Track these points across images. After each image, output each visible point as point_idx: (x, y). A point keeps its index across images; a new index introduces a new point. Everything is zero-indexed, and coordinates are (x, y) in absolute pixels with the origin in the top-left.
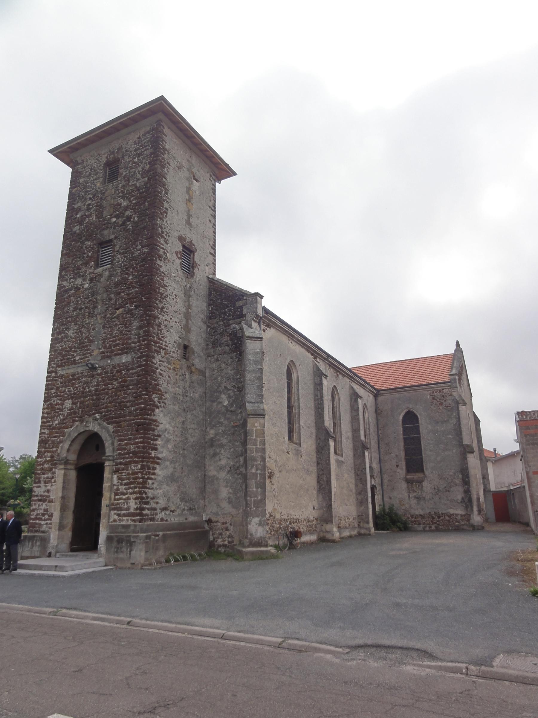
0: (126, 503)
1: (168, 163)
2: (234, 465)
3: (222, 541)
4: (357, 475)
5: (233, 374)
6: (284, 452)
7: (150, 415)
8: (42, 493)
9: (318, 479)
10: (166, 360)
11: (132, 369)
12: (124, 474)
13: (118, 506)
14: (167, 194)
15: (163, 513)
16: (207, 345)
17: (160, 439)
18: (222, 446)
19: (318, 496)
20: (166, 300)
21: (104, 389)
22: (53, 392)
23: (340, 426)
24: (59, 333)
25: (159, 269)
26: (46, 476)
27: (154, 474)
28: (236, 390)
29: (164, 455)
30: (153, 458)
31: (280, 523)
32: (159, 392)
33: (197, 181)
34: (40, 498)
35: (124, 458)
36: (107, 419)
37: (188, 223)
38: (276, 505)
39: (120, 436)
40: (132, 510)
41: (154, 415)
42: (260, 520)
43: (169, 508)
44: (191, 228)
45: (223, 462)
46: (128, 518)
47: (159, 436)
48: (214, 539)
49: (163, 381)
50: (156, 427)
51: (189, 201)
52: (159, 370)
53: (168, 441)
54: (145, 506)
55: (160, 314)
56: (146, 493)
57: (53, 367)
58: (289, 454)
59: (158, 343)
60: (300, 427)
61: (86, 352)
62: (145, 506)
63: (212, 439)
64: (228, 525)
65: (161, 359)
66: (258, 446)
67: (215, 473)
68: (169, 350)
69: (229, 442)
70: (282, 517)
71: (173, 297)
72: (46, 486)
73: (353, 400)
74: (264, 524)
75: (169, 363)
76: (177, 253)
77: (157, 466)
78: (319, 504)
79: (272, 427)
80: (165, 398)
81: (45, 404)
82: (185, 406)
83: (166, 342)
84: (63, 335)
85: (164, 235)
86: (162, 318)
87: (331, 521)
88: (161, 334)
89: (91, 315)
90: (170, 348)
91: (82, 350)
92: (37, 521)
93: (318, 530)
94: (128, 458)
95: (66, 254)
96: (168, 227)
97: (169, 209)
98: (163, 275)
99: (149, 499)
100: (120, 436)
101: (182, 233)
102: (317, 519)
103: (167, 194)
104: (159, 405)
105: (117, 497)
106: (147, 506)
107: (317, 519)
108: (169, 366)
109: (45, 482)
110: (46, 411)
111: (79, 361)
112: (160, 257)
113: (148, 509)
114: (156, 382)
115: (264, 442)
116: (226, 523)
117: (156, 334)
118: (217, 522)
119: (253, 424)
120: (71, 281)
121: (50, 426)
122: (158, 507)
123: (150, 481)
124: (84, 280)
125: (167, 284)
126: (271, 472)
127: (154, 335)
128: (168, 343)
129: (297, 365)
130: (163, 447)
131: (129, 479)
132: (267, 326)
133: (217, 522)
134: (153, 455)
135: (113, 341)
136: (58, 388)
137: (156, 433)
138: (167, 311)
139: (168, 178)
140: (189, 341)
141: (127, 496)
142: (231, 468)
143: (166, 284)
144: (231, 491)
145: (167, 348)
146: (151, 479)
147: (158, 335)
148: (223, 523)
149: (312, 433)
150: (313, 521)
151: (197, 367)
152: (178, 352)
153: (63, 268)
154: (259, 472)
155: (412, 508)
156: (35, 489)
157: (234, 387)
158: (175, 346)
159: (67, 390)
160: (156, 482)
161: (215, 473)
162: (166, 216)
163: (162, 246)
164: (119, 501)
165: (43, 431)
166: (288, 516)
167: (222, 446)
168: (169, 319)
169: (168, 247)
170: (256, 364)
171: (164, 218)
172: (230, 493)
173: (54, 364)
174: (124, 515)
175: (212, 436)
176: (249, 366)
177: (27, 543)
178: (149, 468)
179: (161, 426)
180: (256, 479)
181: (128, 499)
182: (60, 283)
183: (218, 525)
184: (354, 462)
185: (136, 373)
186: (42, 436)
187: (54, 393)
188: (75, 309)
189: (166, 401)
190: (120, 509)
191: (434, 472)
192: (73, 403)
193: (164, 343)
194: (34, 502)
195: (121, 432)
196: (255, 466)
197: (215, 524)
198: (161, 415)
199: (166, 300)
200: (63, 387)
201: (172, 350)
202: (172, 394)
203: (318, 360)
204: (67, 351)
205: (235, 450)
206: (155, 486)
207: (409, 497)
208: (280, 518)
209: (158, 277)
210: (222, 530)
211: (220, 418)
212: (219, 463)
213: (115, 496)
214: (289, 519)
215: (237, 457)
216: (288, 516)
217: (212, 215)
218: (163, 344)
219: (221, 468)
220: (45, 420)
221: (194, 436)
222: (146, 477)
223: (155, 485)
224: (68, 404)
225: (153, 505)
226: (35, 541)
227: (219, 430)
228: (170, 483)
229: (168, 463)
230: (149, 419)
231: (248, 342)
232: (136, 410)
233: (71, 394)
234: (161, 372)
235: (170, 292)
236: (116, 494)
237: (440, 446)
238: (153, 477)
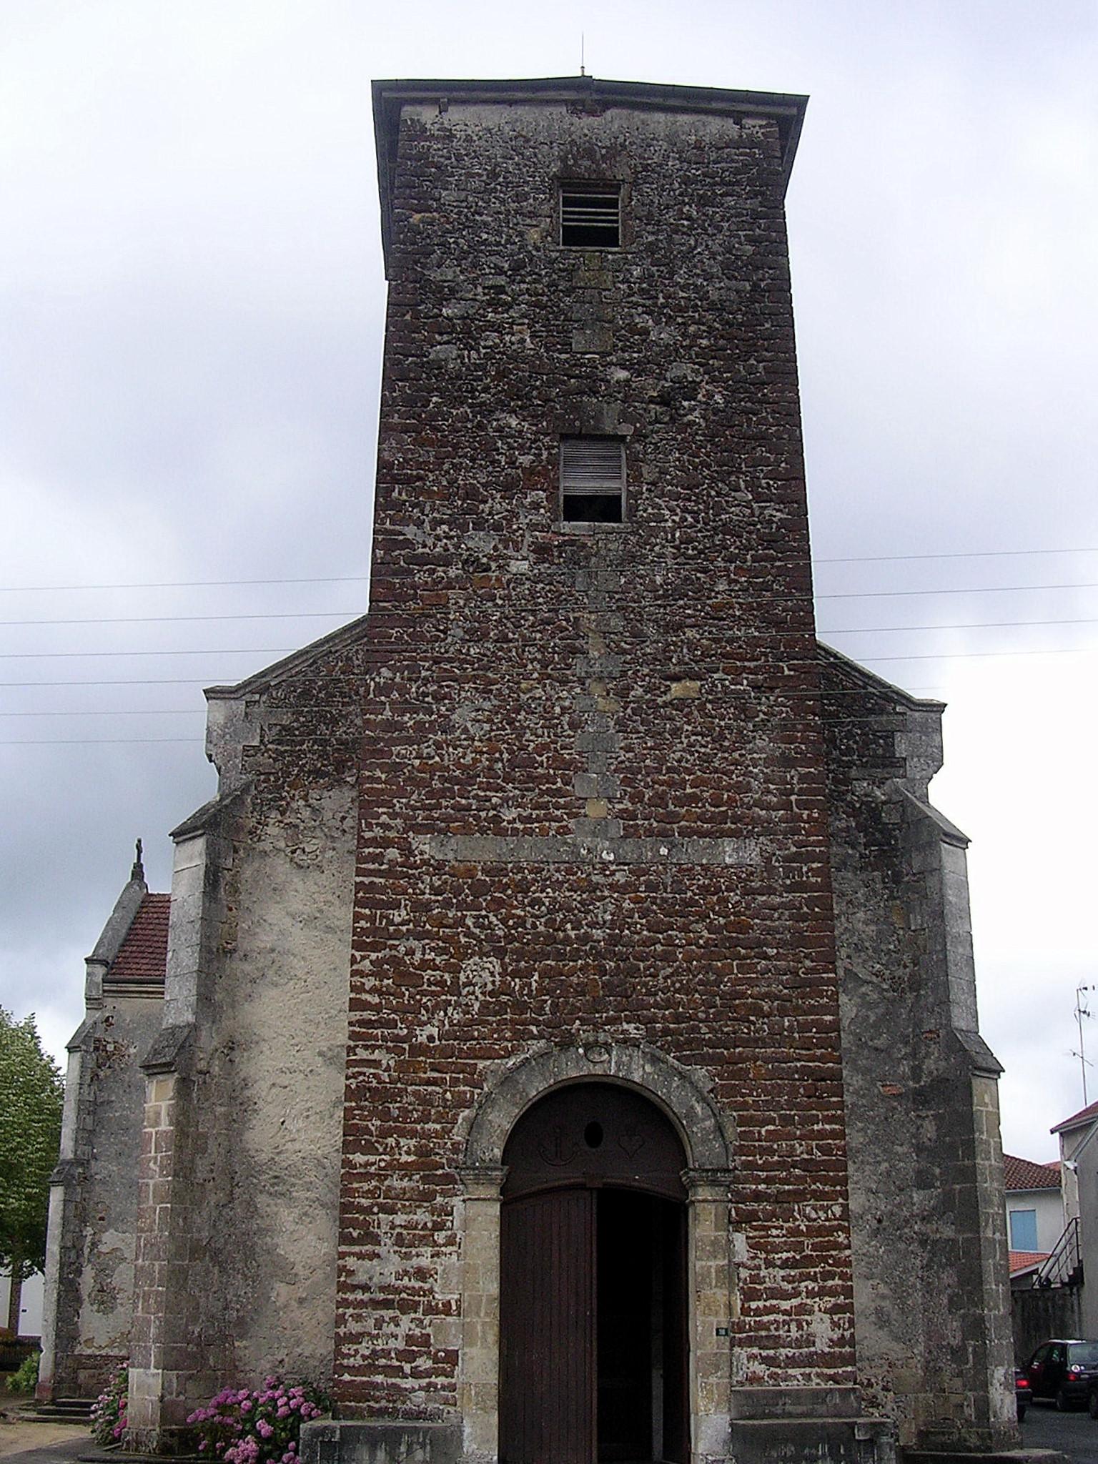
13: (763, 1333)
35: (767, 1181)
40: (821, 1346)
46: (808, 1370)
64: (877, 1389)
94: (785, 1181)
105: (753, 1305)
109: (400, 1241)
174: (792, 1362)
181: (802, 1309)
226: (403, 1448)
231: (948, 852)
236: (750, 1295)
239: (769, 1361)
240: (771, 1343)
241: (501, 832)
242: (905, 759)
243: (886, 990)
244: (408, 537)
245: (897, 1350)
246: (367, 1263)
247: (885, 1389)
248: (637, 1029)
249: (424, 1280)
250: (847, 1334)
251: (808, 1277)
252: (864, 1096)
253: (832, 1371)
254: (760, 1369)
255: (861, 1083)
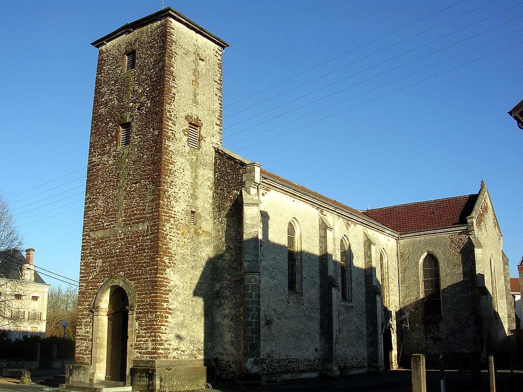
0: (145, 344)
1: (175, 53)
2: (235, 314)
3: (226, 376)
4: (368, 318)
5: (234, 235)
6: (283, 301)
7: (162, 274)
8: (83, 334)
9: (321, 324)
10: (175, 227)
11: (146, 236)
12: (143, 321)
13: (140, 346)
14: (174, 81)
15: (175, 352)
16: (214, 208)
17: (170, 294)
18: (226, 298)
19: (320, 339)
20: (174, 174)
21: (126, 251)
22: (87, 253)
23: (351, 273)
24: (91, 202)
25: (168, 149)
26: (85, 320)
27: (166, 322)
28: (237, 249)
29: (174, 306)
30: (166, 309)
31: (278, 362)
32: (169, 255)
33: (203, 60)
34: (82, 338)
35: (142, 309)
36: (129, 276)
37: (195, 102)
38: (274, 347)
39: (139, 291)
40: (150, 350)
41: (166, 274)
42: (255, 359)
43: (180, 349)
44: (197, 106)
45: (227, 311)
46: (147, 355)
47: (170, 291)
48: (220, 374)
49: (173, 245)
50: (167, 284)
51: (195, 82)
52: (169, 236)
53: (178, 294)
54: (159, 347)
55: (169, 187)
56: (160, 337)
57: (86, 231)
58: (289, 303)
59: (169, 213)
60: (302, 278)
61: (111, 219)
62: (159, 347)
63: (217, 292)
64: (231, 363)
65: (170, 227)
66: (254, 299)
67: (221, 320)
68: (178, 218)
69: (231, 294)
70: (281, 357)
71: (180, 171)
72: (86, 329)
73: (366, 247)
74: (258, 363)
75: (177, 229)
76: (184, 131)
77: (169, 316)
78: (321, 346)
79: (271, 280)
80: (174, 259)
81: (82, 262)
82: (192, 264)
83: (175, 211)
84: (94, 204)
85: (172, 118)
86: (171, 191)
87: (332, 361)
88: (170, 205)
89: (114, 188)
90: (179, 216)
91: (109, 218)
92: (81, 355)
93: (320, 369)
94: (145, 309)
95: (95, 133)
96: (176, 110)
97: (177, 94)
98: (171, 153)
99: (163, 342)
100: (139, 291)
101: (189, 112)
102: (319, 360)
103: (174, 81)
104: (169, 265)
105: (138, 339)
106: (162, 347)
107: (319, 360)
108: (178, 232)
109: (85, 326)
110: (83, 268)
111: (107, 227)
112: (169, 138)
113: (162, 349)
114: (166, 246)
115: (259, 296)
116: (230, 362)
117: (166, 206)
118: (223, 360)
119: (251, 279)
120: (98, 158)
121: (86, 280)
122: (171, 347)
123: (163, 328)
124: (109, 157)
125: (175, 161)
126: (269, 320)
127: (164, 207)
128: (176, 212)
129: (300, 220)
130: (173, 300)
131: (146, 325)
132: (267, 190)
133: (223, 360)
134: (165, 306)
135: (132, 211)
136: (91, 249)
137: (167, 288)
138: (175, 184)
139: (175, 66)
140: (196, 207)
141: (146, 339)
142: (233, 317)
143: (174, 161)
144: (233, 335)
145: (176, 216)
146: (165, 325)
147: (167, 206)
148: (227, 362)
149: (315, 283)
150: (315, 361)
151: (204, 229)
152: (186, 219)
153: (92, 145)
154: (254, 320)
155: (428, 348)
156: (78, 330)
157: (235, 246)
158: (184, 214)
159: (98, 251)
160: (168, 328)
161: (221, 320)
162: (174, 101)
163: (170, 128)
164: (140, 343)
165: (81, 284)
166: (287, 357)
167: (226, 298)
168: (178, 191)
169: (175, 128)
170: (253, 227)
171: (172, 102)
172: (232, 337)
173: (87, 229)
174: (144, 353)
175: (218, 289)
176: (247, 229)
177: (75, 372)
178: (162, 317)
179: (172, 283)
180: (252, 326)
181: (147, 341)
182: (90, 159)
183: (223, 363)
184: (367, 306)
185: (149, 239)
186: (81, 288)
187: (88, 253)
188: (103, 182)
189: (175, 262)
190: (141, 348)
191: (450, 314)
192: (103, 263)
193: (173, 213)
194: (78, 341)
195: (139, 288)
196: (251, 316)
197: (220, 362)
198: (172, 273)
199: (174, 174)
200: (95, 248)
201: (180, 218)
202: (181, 255)
203: (325, 212)
204: (97, 218)
205: (236, 301)
206: (167, 331)
207: (426, 338)
208: (278, 358)
209: (167, 156)
210: (226, 367)
211: (224, 274)
212: (224, 312)
213: (137, 338)
214: (288, 359)
215: (238, 307)
216: (287, 357)
217: (218, 89)
218: (172, 213)
219: (226, 316)
220: (82, 275)
221: (202, 289)
222: (160, 324)
223: (167, 330)
224: (99, 262)
225: (167, 346)
226: (80, 371)
227: (223, 284)
228: (180, 329)
229: (178, 313)
230: (161, 278)
231: (246, 208)
232: (151, 270)
233: (101, 255)
234: (171, 237)
235: (178, 167)
236: (138, 337)
237: (457, 288)
238: (166, 324)
239: (140, 353)
240: (140, 349)
241: (104, 229)
242: (245, 182)
243: (237, 251)
244: (93, 160)
245: (235, 352)
246: (80, 330)
247: (233, 363)
248: (123, 273)
249: (88, 334)
250: (154, 347)
251: (148, 333)
252: (230, 282)
253: (151, 356)
254: (139, 355)
255: (230, 278)
